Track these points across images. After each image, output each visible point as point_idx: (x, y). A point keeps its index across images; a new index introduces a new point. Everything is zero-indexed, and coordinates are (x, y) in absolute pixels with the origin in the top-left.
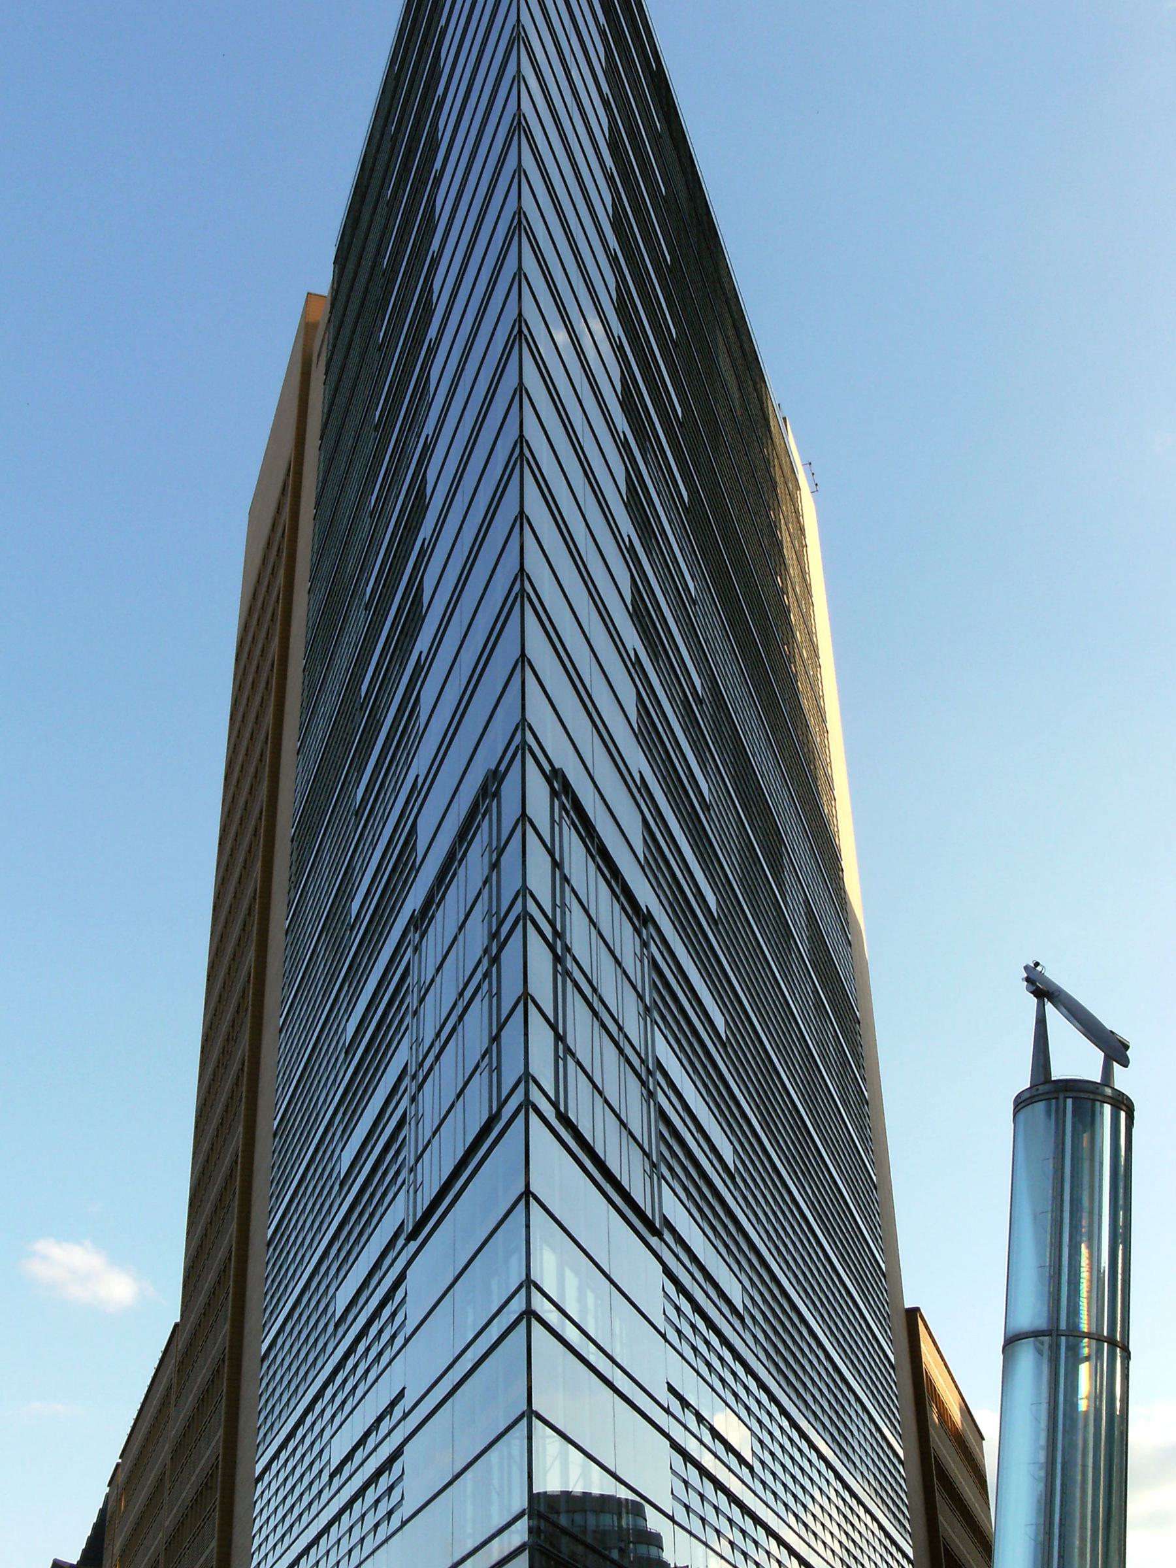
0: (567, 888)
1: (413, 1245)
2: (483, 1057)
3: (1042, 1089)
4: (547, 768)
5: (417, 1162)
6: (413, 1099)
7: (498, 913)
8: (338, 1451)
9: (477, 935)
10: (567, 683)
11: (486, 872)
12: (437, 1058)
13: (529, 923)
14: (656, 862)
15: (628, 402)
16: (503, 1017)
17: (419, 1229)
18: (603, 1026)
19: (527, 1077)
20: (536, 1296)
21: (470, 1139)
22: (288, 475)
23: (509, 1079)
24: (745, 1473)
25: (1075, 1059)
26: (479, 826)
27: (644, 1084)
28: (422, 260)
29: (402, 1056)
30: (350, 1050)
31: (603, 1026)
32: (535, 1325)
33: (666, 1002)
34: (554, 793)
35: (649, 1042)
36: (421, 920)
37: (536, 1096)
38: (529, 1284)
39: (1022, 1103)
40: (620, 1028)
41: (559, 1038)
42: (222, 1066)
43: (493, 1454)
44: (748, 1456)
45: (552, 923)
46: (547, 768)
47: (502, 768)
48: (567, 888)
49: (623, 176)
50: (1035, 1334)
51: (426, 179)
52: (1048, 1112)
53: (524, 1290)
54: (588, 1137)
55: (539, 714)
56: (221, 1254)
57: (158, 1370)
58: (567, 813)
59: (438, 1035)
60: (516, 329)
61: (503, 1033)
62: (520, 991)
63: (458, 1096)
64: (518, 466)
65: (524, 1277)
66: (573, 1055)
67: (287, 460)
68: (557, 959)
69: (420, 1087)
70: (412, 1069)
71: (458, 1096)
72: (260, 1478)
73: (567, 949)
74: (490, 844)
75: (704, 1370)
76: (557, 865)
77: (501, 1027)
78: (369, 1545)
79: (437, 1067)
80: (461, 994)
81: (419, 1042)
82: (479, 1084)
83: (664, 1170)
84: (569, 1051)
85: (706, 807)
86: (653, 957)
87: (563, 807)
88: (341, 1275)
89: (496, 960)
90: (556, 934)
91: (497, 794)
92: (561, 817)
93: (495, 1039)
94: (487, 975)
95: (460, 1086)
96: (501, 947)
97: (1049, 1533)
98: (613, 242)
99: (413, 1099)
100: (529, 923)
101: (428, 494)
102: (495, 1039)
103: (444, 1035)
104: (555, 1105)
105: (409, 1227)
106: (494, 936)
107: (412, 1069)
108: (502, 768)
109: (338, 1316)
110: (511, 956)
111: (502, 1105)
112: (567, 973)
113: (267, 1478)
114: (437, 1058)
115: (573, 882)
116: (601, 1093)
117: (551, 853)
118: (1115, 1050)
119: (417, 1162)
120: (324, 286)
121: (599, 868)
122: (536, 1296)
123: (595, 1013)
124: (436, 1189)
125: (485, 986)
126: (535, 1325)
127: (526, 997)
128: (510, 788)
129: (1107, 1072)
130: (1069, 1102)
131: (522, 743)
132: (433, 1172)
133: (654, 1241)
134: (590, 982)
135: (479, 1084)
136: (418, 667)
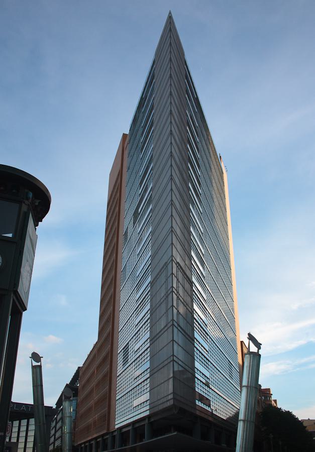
19: (173, 287)
23: (169, 320)
24: (207, 352)
25: (253, 349)
30: (140, 194)
34: (177, 267)
37: (174, 290)
42: (110, 209)
44: (208, 350)
53: (172, 327)
56: (110, 295)
57: (91, 351)
62: (172, 354)
67: (118, 171)
72: (119, 376)
75: (201, 363)
78: (143, 363)
85: (202, 233)
89: (167, 297)
94: (165, 299)
97: (246, 409)
104: (177, 323)
106: (167, 267)
112: (179, 299)
113: (120, 377)
118: (258, 345)
120: (127, 132)
122: (175, 357)
128: (170, 266)
129: (258, 351)
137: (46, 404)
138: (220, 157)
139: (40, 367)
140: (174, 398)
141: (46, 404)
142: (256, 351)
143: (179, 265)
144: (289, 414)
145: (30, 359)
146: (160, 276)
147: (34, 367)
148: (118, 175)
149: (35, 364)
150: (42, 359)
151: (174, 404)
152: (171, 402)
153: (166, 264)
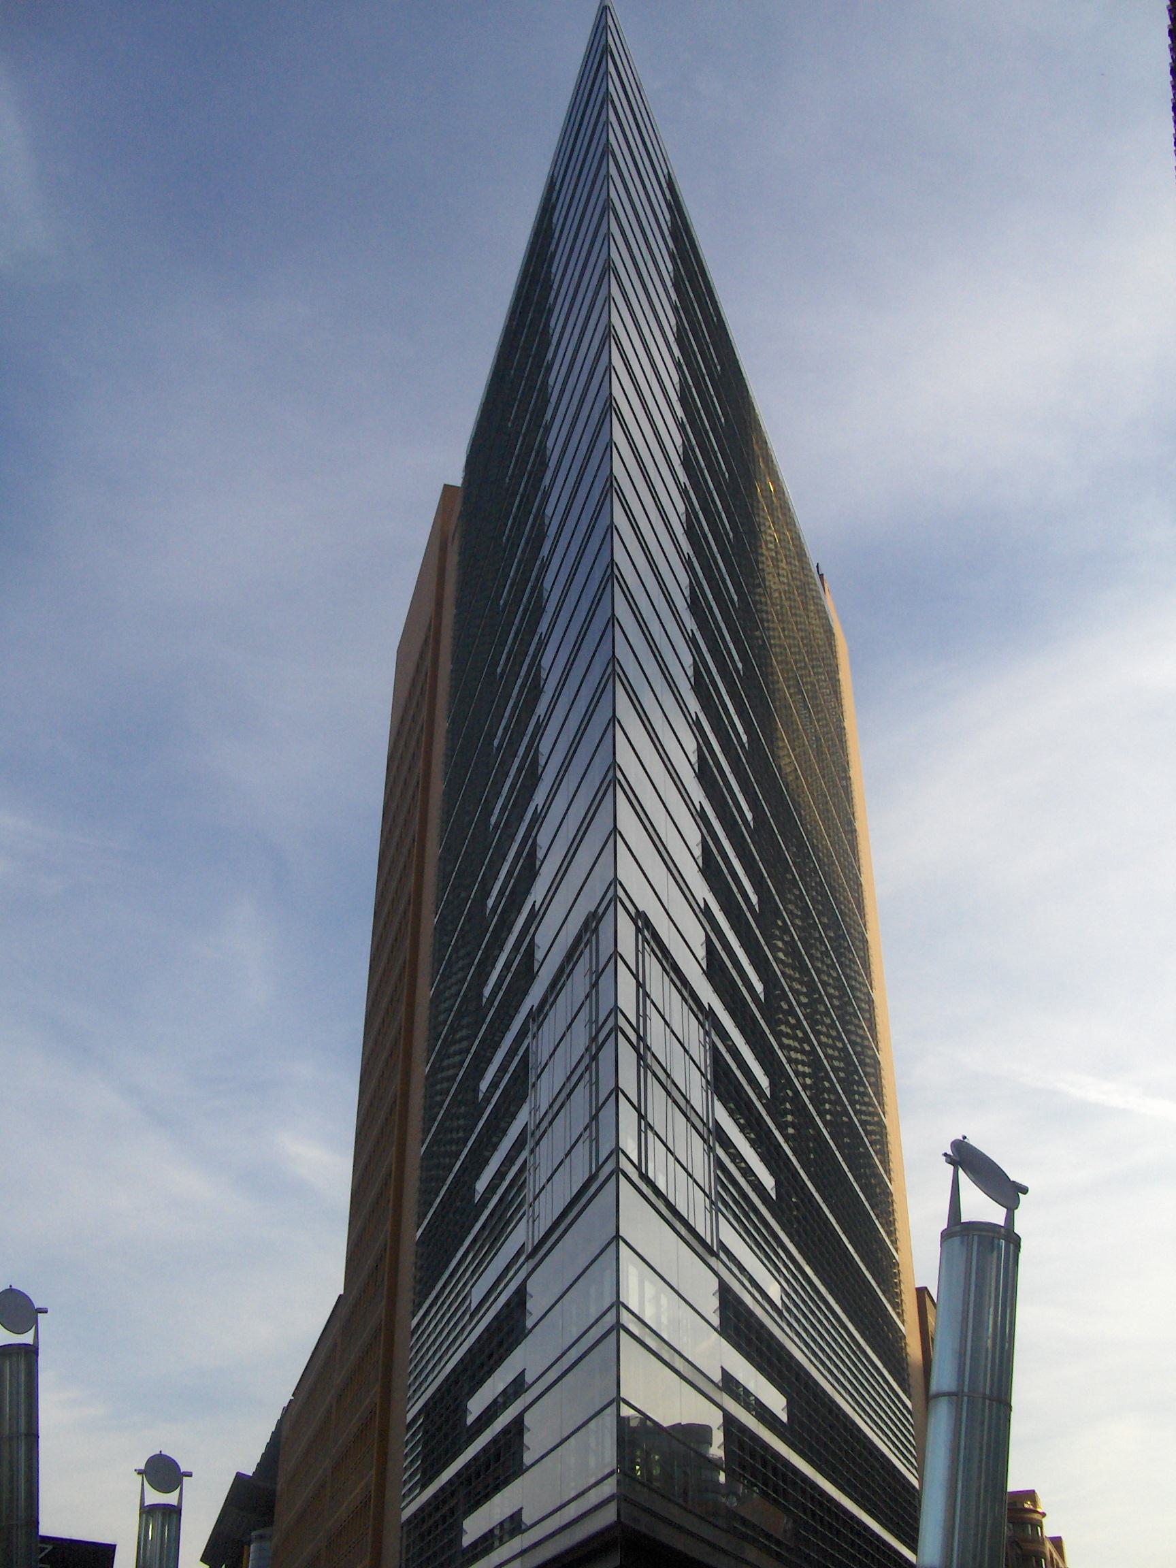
0: (648, 1001)
1: (532, 1263)
2: (585, 1129)
3: (958, 1228)
4: (633, 911)
5: (535, 1199)
6: (532, 1151)
7: (597, 1021)
8: (476, 1298)
9: (580, 1038)
10: (648, 847)
11: (588, 990)
12: (551, 1123)
13: (619, 1034)
14: (715, 970)
15: (695, 606)
16: (600, 1102)
17: (539, 1250)
18: (675, 1102)
20: (624, 1312)
21: (575, 1192)
22: (429, 630)
23: (605, 1149)
25: (980, 1207)
26: (582, 953)
27: (705, 1141)
28: (539, 426)
29: (523, 1117)
31: (675, 1102)
32: (622, 1333)
33: (723, 1082)
34: (638, 930)
35: (709, 1108)
36: (538, 1015)
38: (618, 1304)
39: (946, 1236)
40: (688, 1102)
41: (642, 1117)
43: (592, 1424)
45: (636, 1031)
46: (633, 911)
47: (601, 911)
48: (648, 1001)
49: (691, 421)
50: (948, 1394)
51: (541, 366)
52: (962, 1242)
54: (663, 1190)
55: (627, 872)
58: (648, 944)
59: (551, 1106)
60: (609, 570)
61: (601, 1114)
63: (566, 1156)
64: (611, 789)
65: (614, 1299)
66: (652, 1128)
68: (640, 1057)
69: (537, 1143)
70: (531, 1127)
71: (566, 1156)
73: (648, 1048)
74: (591, 968)
76: (640, 985)
77: (598, 1110)
79: (550, 1130)
80: (569, 1078)
81: (536, 1109)
82: (582, 1150)
83: (720, 1205)
84: (648, 1125)
86: (714, 1043)
87: (645, 939)
88: (478, 1272)
89: (594, 1058)
90: (639, 1038)
91: (596, 931)
92: (643, 948)
93: (595, 1117)
94: (588, 1068)
95: (568, 1148)
96: (599, 1049)
98: (683, 478)
99: (532, 1151)
100: (619, 1034)
101: (542, 762)
102: (595, 1117)
103: (556, 1107)
104: (638, 1168)
105: (529, 1249)
106: (594, 1039)
107: (531, 1127)
108: (601, 911)
109: (473, 1307)
110: (606, 1054)
111: (599, 1168)
112: (647, 1067)
114: (551, 1123)
115: (652, 997)
116: (672, 1154)
117: (636, 977)
118: (1007, 1192)
119: (535, 1199)
120: (457, 479)
121: (672, 980)
122: (624, 1312)
123: (669, 1093)
124: (549, 1224)
125: (587, 1075)
126: (622, 1333)
127: (617, 1089)
129: (1010, 1218)
130: (976, 1238)
131: (614, 894)
132: (548, 1208)
133: (713, 1261)
134: (665, 1071)
135: (582, 1150)
136: (533, 914)
137: (43, 1531)
138: (821, 576)
139: (30, 1353)
140: (620, 1498)
141: (43, 1531)
142: (1000, 1221)
143: (648, 924)
144: (1171, 33)
145: (140, 1477)
146: (569, 976)
147: (148, 1512)
148: (426, 642)
149: (155, 1497)
150: (185, 1478)
151: (618, 1522)
152: (608, 1516)
153: (592, 923)
